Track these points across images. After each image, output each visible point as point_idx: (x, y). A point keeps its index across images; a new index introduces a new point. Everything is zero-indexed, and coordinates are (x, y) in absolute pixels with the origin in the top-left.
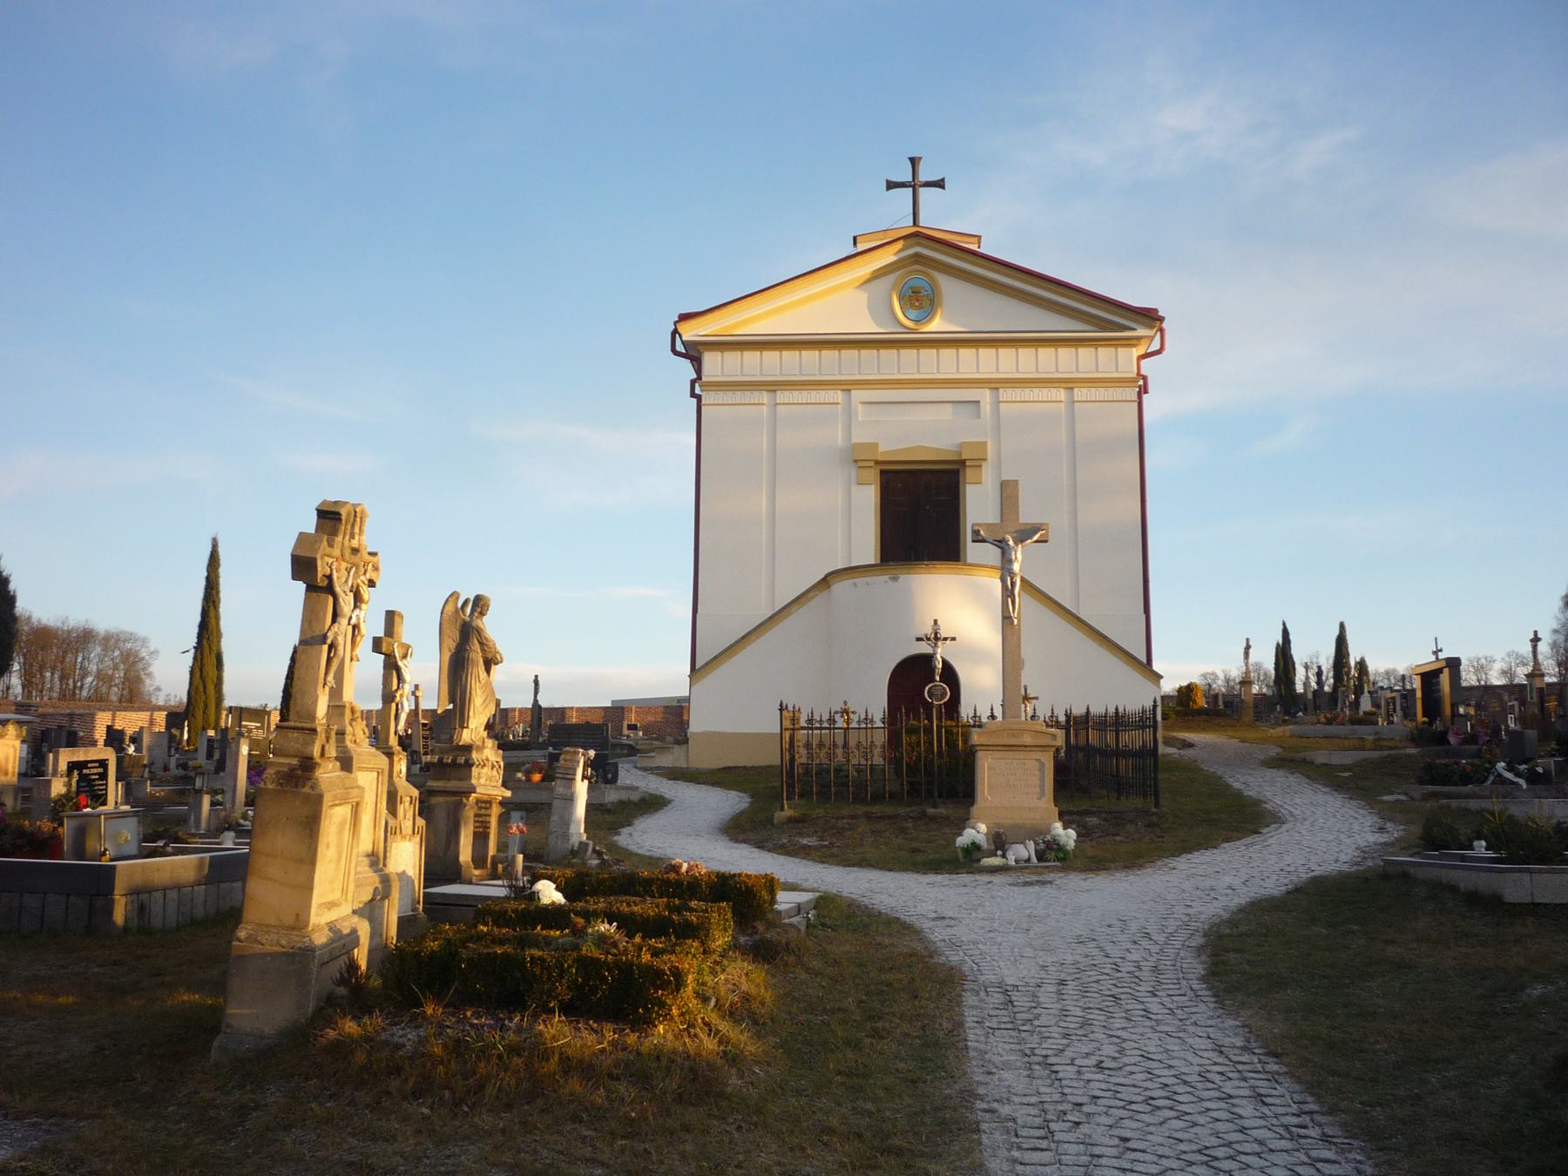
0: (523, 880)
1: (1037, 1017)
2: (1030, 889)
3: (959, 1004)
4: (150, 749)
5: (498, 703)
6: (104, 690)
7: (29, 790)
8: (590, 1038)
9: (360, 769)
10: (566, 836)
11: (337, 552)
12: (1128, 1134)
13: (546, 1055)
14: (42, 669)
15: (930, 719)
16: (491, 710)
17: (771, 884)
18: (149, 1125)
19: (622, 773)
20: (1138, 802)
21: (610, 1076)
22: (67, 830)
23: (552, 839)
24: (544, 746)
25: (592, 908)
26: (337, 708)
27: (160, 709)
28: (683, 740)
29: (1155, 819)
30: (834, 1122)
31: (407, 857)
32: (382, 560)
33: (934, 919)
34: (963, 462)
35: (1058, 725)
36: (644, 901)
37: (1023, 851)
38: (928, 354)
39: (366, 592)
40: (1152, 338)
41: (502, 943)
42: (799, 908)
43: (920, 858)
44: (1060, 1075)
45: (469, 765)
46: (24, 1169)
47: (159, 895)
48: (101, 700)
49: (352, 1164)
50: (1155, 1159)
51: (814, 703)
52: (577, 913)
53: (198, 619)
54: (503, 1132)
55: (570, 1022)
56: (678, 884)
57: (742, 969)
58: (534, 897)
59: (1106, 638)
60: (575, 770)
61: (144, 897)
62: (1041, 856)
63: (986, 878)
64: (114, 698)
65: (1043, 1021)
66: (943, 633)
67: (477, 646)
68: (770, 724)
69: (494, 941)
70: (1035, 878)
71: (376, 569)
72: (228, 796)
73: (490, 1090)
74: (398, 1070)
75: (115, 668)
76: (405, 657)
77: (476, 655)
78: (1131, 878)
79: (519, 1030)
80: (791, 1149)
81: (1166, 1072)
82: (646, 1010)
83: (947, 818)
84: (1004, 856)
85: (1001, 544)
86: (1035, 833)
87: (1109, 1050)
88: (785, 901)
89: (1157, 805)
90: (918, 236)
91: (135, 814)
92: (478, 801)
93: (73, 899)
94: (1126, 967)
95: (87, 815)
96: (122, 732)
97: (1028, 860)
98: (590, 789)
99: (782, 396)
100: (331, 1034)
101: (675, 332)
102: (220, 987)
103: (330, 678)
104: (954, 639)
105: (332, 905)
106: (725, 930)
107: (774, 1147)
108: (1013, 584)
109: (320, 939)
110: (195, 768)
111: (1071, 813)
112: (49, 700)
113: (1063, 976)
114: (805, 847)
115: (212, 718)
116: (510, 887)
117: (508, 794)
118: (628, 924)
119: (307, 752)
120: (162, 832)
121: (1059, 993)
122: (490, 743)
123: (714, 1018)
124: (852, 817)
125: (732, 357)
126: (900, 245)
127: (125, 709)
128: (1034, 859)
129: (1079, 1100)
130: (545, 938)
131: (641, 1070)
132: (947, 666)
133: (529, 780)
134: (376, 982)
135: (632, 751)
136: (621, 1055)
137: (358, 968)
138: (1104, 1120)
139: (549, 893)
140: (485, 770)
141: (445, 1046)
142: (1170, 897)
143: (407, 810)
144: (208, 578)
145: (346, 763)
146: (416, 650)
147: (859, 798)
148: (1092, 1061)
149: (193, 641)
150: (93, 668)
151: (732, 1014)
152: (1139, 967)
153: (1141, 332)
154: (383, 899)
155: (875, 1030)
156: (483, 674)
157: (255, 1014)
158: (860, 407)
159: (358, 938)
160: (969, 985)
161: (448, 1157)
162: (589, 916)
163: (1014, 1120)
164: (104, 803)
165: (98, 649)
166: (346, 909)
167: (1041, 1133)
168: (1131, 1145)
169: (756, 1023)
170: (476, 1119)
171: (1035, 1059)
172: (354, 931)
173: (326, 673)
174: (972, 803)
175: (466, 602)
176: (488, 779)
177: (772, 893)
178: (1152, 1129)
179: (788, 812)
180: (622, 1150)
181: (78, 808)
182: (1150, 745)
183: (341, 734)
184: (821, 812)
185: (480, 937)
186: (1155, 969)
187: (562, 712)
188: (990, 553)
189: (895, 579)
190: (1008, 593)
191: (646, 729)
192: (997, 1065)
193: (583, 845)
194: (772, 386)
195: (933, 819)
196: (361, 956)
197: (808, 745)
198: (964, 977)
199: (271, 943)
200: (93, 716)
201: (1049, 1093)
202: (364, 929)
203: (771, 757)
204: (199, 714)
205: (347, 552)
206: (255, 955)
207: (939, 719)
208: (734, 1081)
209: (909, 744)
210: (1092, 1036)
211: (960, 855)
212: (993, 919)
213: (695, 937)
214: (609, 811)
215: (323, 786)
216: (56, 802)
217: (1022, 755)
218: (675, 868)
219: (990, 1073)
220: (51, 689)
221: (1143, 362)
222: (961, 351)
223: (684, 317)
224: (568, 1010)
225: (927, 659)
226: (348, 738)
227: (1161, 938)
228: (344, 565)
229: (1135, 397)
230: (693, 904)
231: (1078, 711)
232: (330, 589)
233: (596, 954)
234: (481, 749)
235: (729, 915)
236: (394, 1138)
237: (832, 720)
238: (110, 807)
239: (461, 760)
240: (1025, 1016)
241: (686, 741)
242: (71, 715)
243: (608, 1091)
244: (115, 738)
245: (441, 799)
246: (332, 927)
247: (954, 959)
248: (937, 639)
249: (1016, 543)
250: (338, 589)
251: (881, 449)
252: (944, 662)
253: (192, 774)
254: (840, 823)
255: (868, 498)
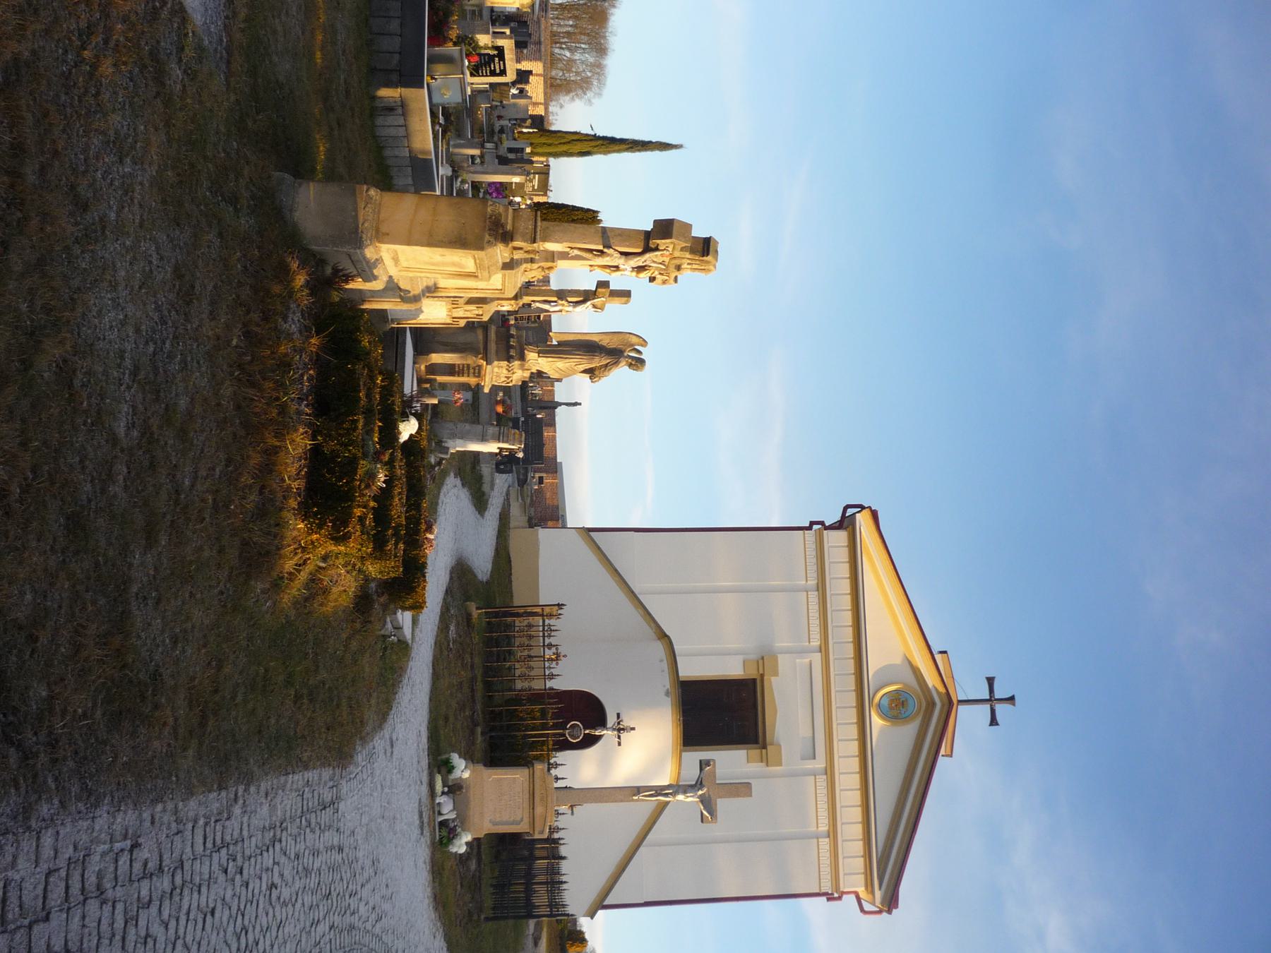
0: (417, 406)
1: (313, 831)
2: (416, 817)
3: (323, 765)
4: (515, 104)
5: (559, 380)
6: (560, 65)
7: (481, 15)
8: (293, 470)
9: (504, 276)
10: (454, 436)
11: (677, 254)
12: (217, 915)
13: (280, 435)
14: (576, 18)
15: (555, 727)
16: (553, 375)
17: (418, 607)
18: (223, 129)
19: (504, 476)
20: (489, 902)
21: (263, 487)
22: (450, 49)
23: (450, 425)
24: (525, 412)
25: (397, 464)
26: (552, 257)
27: (546, 109)
28: (532, 524)
29: (475, 917)
30: (227, 670)
31: (434, 313)
32: (671, 286)
33: (391, 739)
34: (764, 747)
35: (551, 832)
36: (403, 506)
37: (448, 809)
38: (852, 716)
39: (645, 275)
40: (874, 904)
41: (368, 396)
42: (398, 628)
43: (441, 722)
44: (265, 854)
45: (509, 359)
46: (186, 35)
47: (401, 122)
48: (552, 64)
49: (193, 287)
50: (197, 939)
51: (565, 630)
52: (392, 454)
53: (618, 137)
54: (219, 404)
55: (305, 453)
56: (417, 532)
57: (350, 587)
58: (405, 416)
59: (624, 870)
60: (507, 442)
61: (400, 111)
62: (443, 824)
63: (425, 779)
64: (553, 73)
65: (309, 835)
66: (624, 735)
67: (604, 362)
68: (546, 597)
69: (369, 389)
70: (426, 820)
71: (664, 282)
72: (479, 168)
73: (251, 392)
74: (266, 319)
75: (577, 73)
76: (594, 306)
77: (597, 362)
78: (427, 901)
79: (299, 413)
80: (205, 636)
81: (268, 943)
82: (316, 514)
83: (473, 743)
84: (443, 793)
85: (699, 784)
86: (463, 820)
87: (286, 893)
88: (405, 618)
89: (487, 919)
90: (949, 704)
91: (464, 101)
92: (480, 367)
93: (397, 57)
94: (353, 903)
95: (462, 61)
96: (527, 82)
97: (440, 814)
98: (491, 454)
99: (814, 597)
100: (294, 265)
101: (862, 507)
102: (331, 176)
103: (576, 252)
104: (619, 744)
105: (396, 260)
106: (381, 572)
107: (207, 622)
108: (666, 795)
109: (369, 253)
110: (500, 140)
111: (479, 847)
112: (552, 24)
113: (346, 850)
114: (447, 628)
115: (540, 150)
116: (412, 396)
117: (486, 390)
118: (384, 496)
119: (517, 236)
120: (450, 121)
121: (332, 848)
122: (527, 374)
123: (310, 567)
124: (472, 666)
125: (843, 555)
126: (942, 690)
127: (545, 82)
128: (441, 818)
129: (245, 872)
130: (372, 430)
131: (268, 511)
132: (598, 738)
133: (498, 403)
134: (335, 297)
135: (522, 482)
136: (280, 495)
137: (347, 282)
138: (229, 893)
139: (408, 429)
140: (505, 371)
141: (286, 355)
142: (411, 935)
143: (472, 312)
144: (650, 142)
145: (509, 266)
146: (599, 315)
147: (487, 671)
148: (277, 880)
149: (601, 133)
150: (577, 56)
151: (313, 580)
152: (353, 913)
153: (878, 894)
154: (401, 297)
155: (302, 696)
156: (582, 367)
157: (309, 204)
158: (807, 660)
159: (370, 281)
160: (338, 771)
161: (198, 363)
162: (390, 464)
163: (228, 819)
164: (472, 75)
165: (591, 60)
166: (393, 271)
167: (219, 841)
168: (209, 917)
169: (306, 599)
170: (228, 382)
171: (278, 833)
172: (375, 278)
173: (580, 249)
174: (485, 765)
175: (639, 352)
176: (497, 374)
177: (411, 608)
178: (222, 933)
179: (475, 613)
180: (203, 500)
181: (467, 56)
182: (536, 912)
183: (532, 261)
184: (476, 640)
185: (372, 378)
186: (352, 927)
187: (552, 424)
188: (691, 774)
189: (667, 694)
190: (659, 791)
191: (539, 491)
192: (275, 799)
193: (446, 450)
194: (821, 587)
195: (473, 732)
196: (357, 284)
197: (530, 626)
198: (344, 767)
199: (365, 215)
200: (540, 59)
201: (251, 846)
202: (377, 285)
203: (520, 598)
204: (543, 140)
205: (677, 262)
206: (355, 202)
207: (554, 735)
208: (259, 586)
209: (532, 711)
210: (297, 878)
211: (444, 757)
212: (391, 787)
213: (374, 549)
214: (474, 468)
215: (490, 250)
216: (472, 39)
217: (526, 805)
218: (429, 529)
219: (267, 795)
220: (559, 25)
221: (853, 897)
222: (856, 743)
223: (875, 515)
224: (315, 452)
225: (602, 723)
226: (529, 266)
227: (377, 930)
228: (667, 260)
229: (823, 891)
230: (401, 546)
231: (563, 851)
232: (647, 249)
233: (360, 472)
234: (522, 368)
235: (392, 575)
236: (214, 319)
237: (550, 646)
238: (469, 79)
239: (512, 353)
240: (313, 821)
241: (531, 526)
242: (539, 43)
243: (251, 487)
244: (523, 76)
245: (481, 337)
246: (379, 261)
247: (359, 758)
248: (619, 730)
249: (700, 797)
250: (647, 256)
251: (773, 679)
252: (599, 737)
253: (496, 139)
254: (467, 656)
255: (733, 669)
